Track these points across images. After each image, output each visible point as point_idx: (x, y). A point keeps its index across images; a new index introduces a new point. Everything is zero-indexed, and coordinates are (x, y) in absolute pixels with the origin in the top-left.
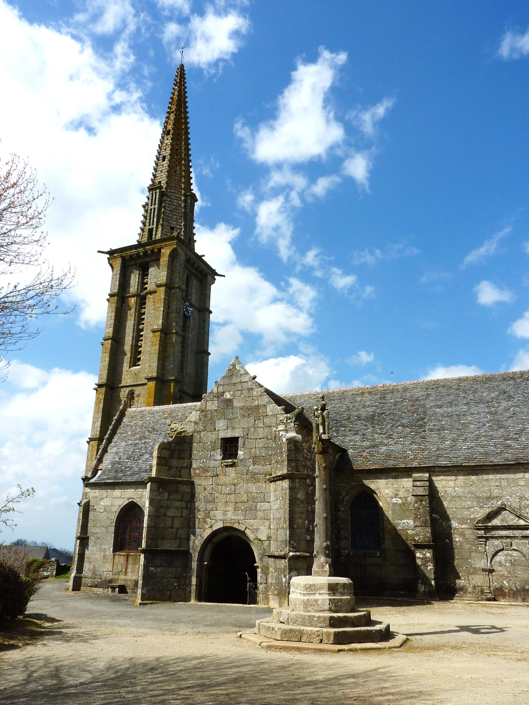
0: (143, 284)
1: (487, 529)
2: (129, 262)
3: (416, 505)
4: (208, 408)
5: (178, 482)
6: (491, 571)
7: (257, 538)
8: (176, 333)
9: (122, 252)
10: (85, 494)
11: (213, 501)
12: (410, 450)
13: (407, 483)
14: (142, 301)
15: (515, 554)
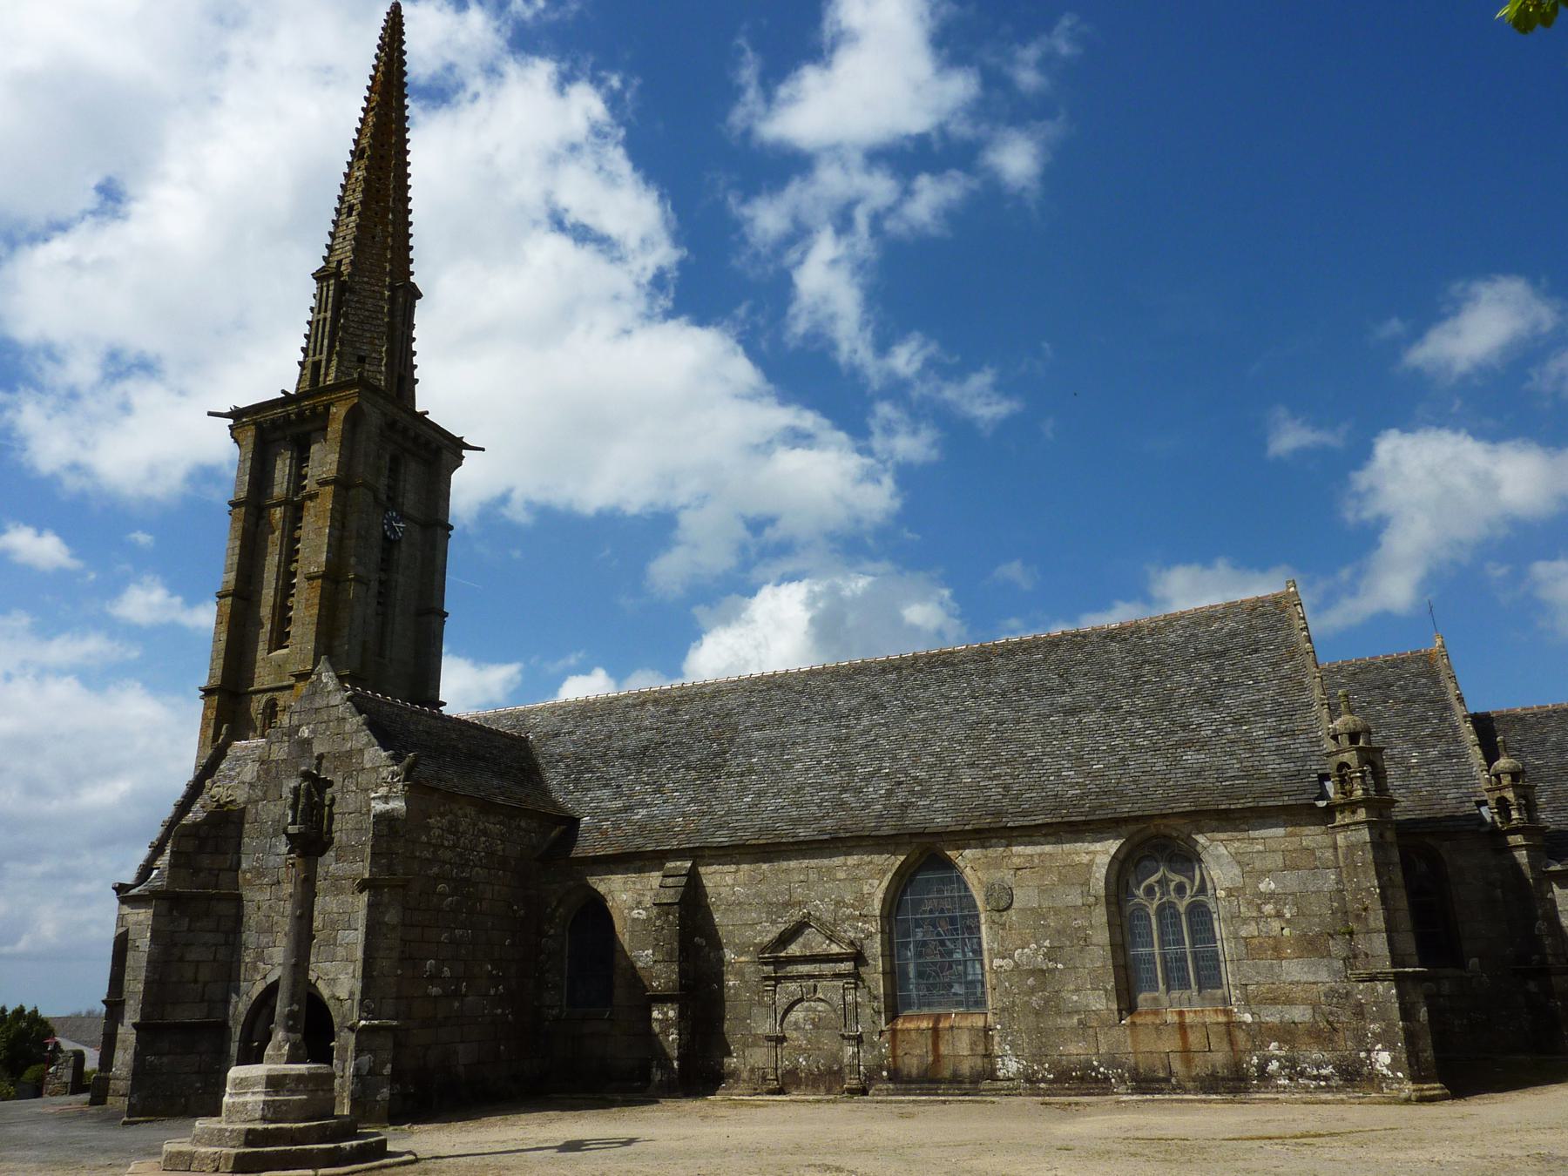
0: (298, 477)
1: (779, 963)
2: (268, 430)
3: (658, 923)
4: (273, 757)
5: (211, 897)
6: (780, 1040)
7: (333, 997)
8: (358, 579)
9: (256, 413)
10: (121, 918)
11: (270, 930)
12: (683, 815)
13: (655, 878)
14: (295, 513)
15: (821, 1006)
